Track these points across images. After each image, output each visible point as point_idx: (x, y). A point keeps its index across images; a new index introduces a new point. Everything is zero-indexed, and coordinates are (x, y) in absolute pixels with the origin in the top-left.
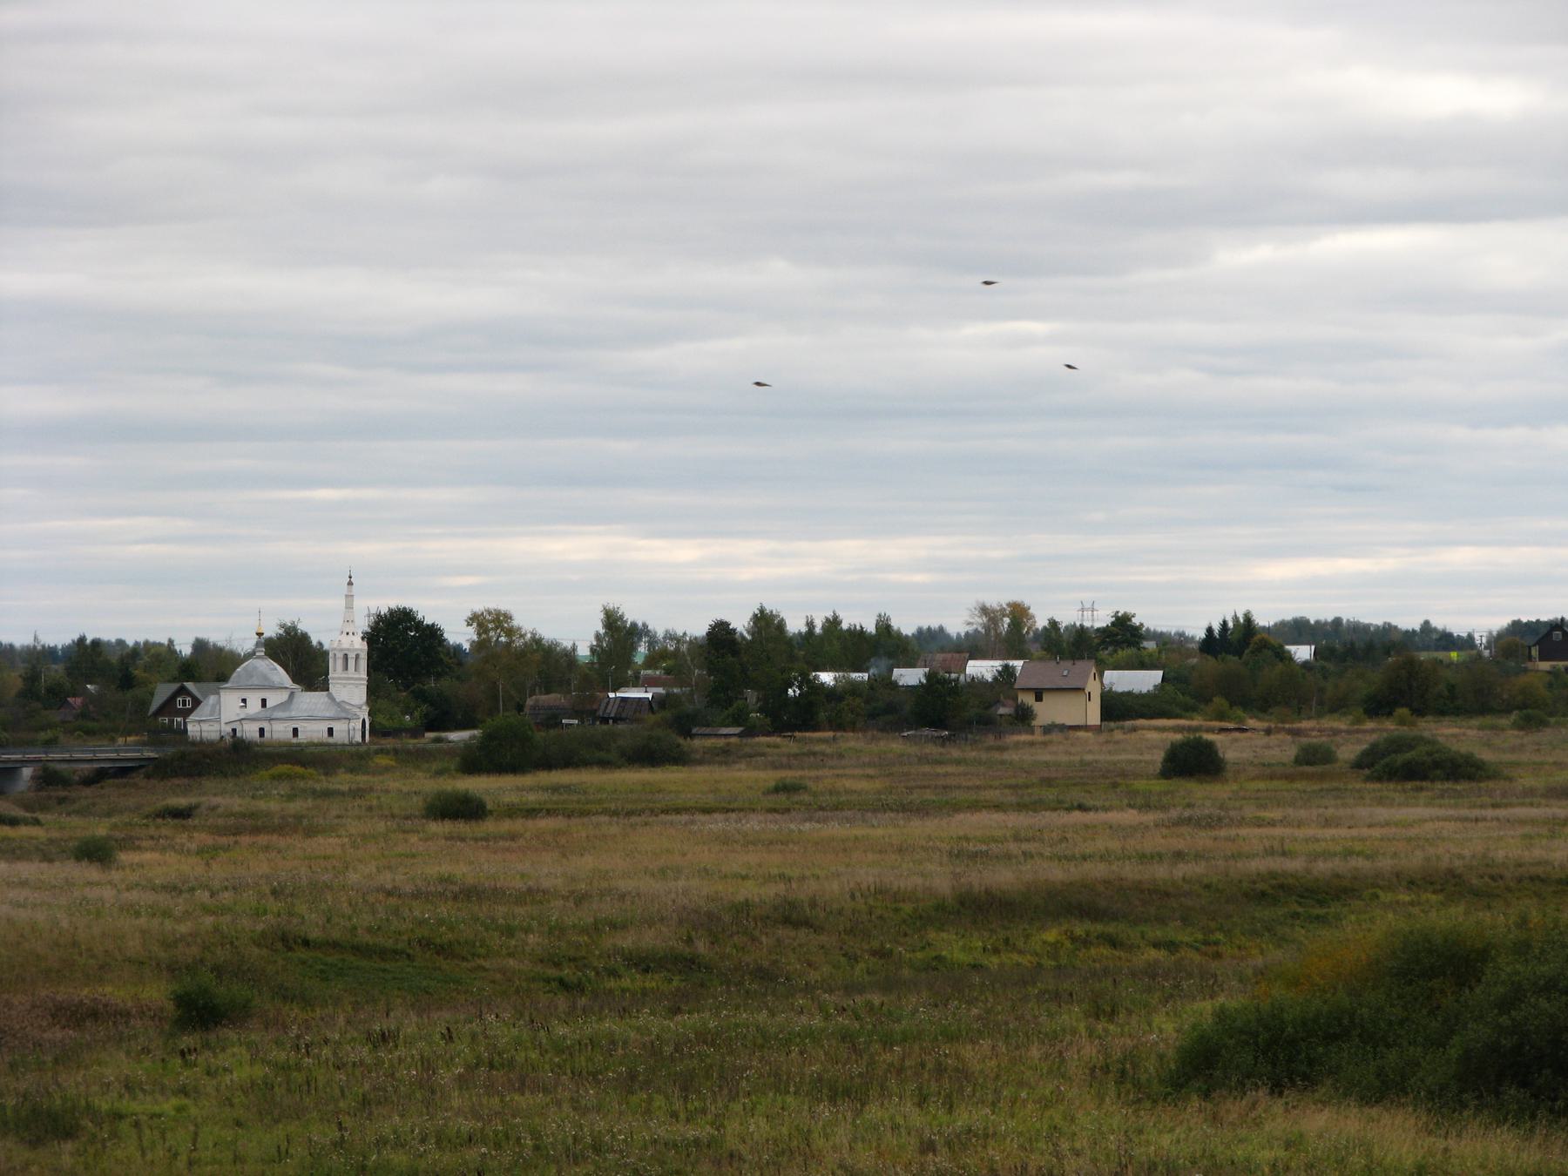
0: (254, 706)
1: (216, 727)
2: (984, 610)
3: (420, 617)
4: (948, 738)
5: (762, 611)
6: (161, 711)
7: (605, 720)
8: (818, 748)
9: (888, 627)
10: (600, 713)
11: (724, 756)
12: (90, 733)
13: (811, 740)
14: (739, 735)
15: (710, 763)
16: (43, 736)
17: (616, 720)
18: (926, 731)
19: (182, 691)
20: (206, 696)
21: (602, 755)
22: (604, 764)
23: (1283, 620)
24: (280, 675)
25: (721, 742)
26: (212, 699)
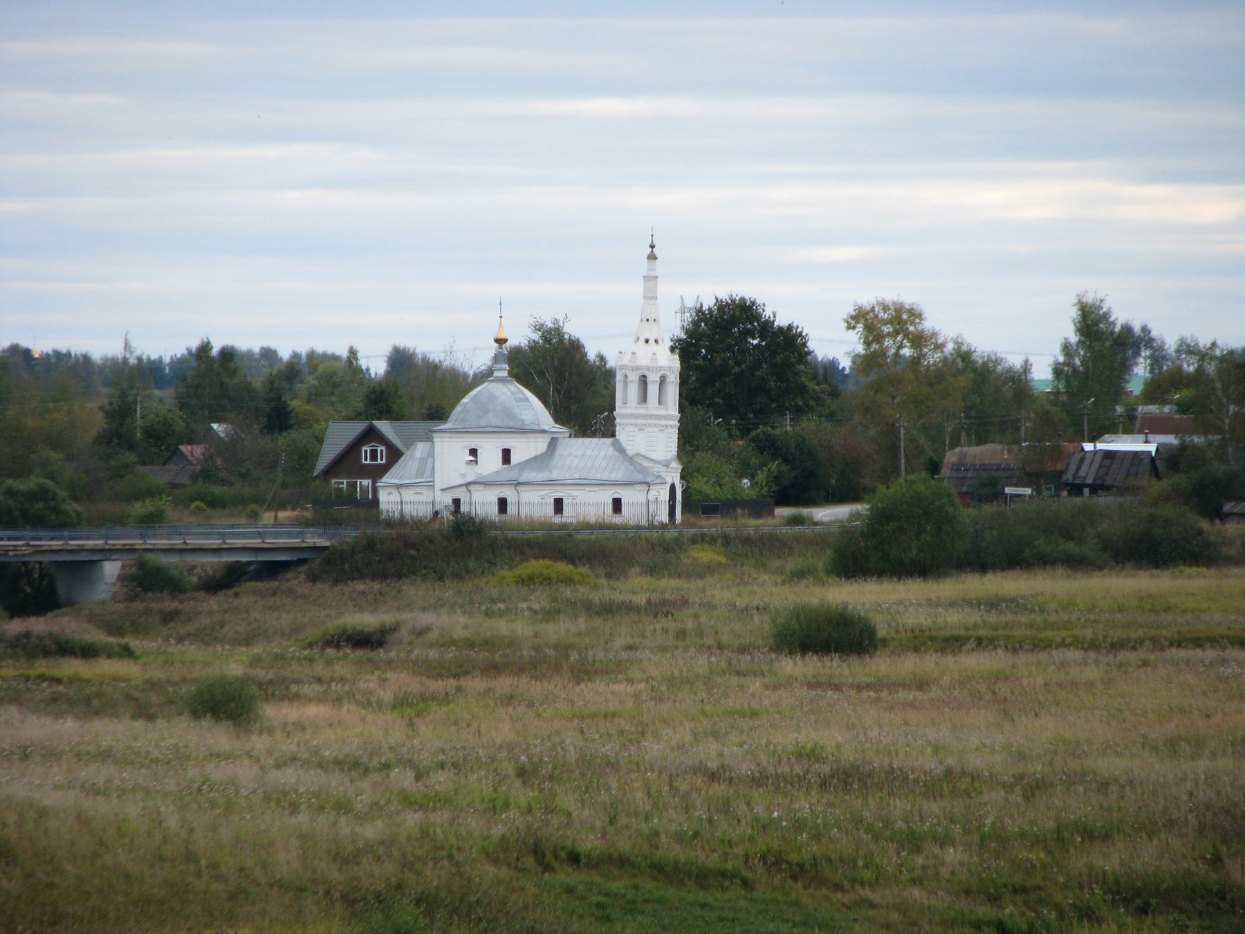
0: (490, 462)
1: (426, 496)
3: (767, 313)
6: (334, 468)
7: (1076, 489)
10: (1069, 477)
12: (216, 503)
17: (1095, 489)
19: (371, 435)
21: (1071, 547)
22: (1075, 563)
26: (420, 449)
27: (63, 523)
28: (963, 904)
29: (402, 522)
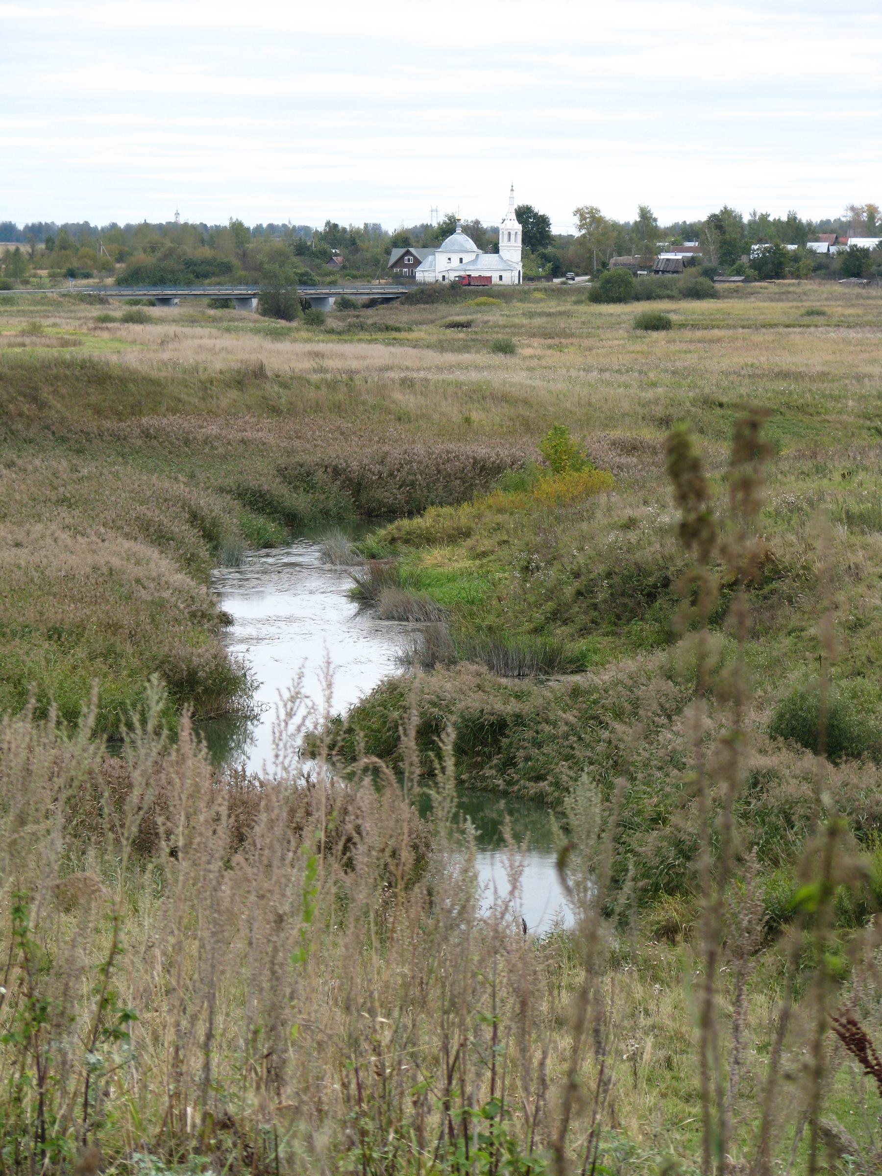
0: (455, 263)
1: (433, 274)
2: (853, 209)
3: (536, 210)
4: (868, 284)
5: (725, 208)
6: (395, 265)
7: (657, 272)
8: (791, 289)
9: (795, 218)
10: (654, 268)
11: (735, 293)
12: (355, 277)
13: (785, 284)
14: (742, 281)
15: (731, 298)
16: (328, 279)
17: (663, 272)
18: (853, 280)
19: (408, 253)
20: (425, 257)
21: (669, 292)
22: (671, 298)
23: (86, 224)
24: (471, 244)
25: (733, 285)
26: (430, 258)
27: (314, 284)
28: (861, 421)
29: (425, 284)
